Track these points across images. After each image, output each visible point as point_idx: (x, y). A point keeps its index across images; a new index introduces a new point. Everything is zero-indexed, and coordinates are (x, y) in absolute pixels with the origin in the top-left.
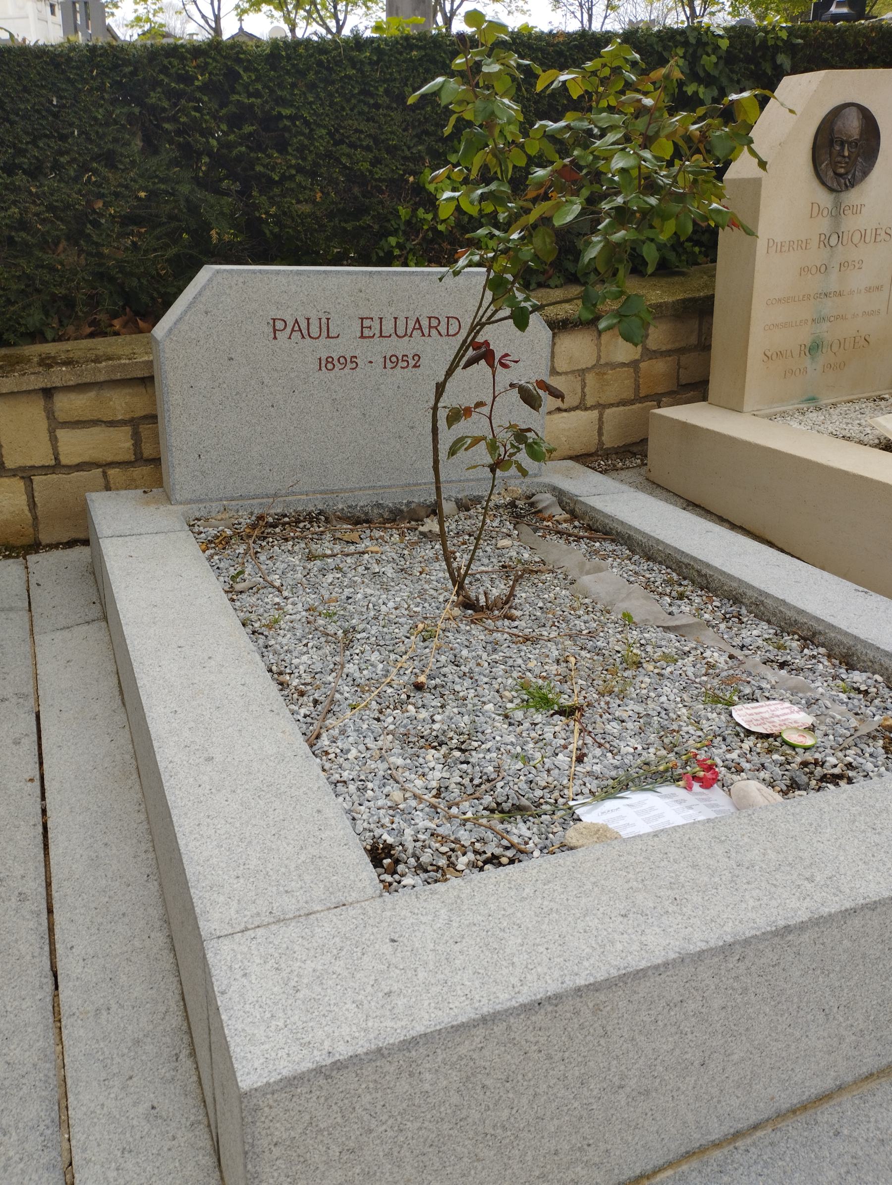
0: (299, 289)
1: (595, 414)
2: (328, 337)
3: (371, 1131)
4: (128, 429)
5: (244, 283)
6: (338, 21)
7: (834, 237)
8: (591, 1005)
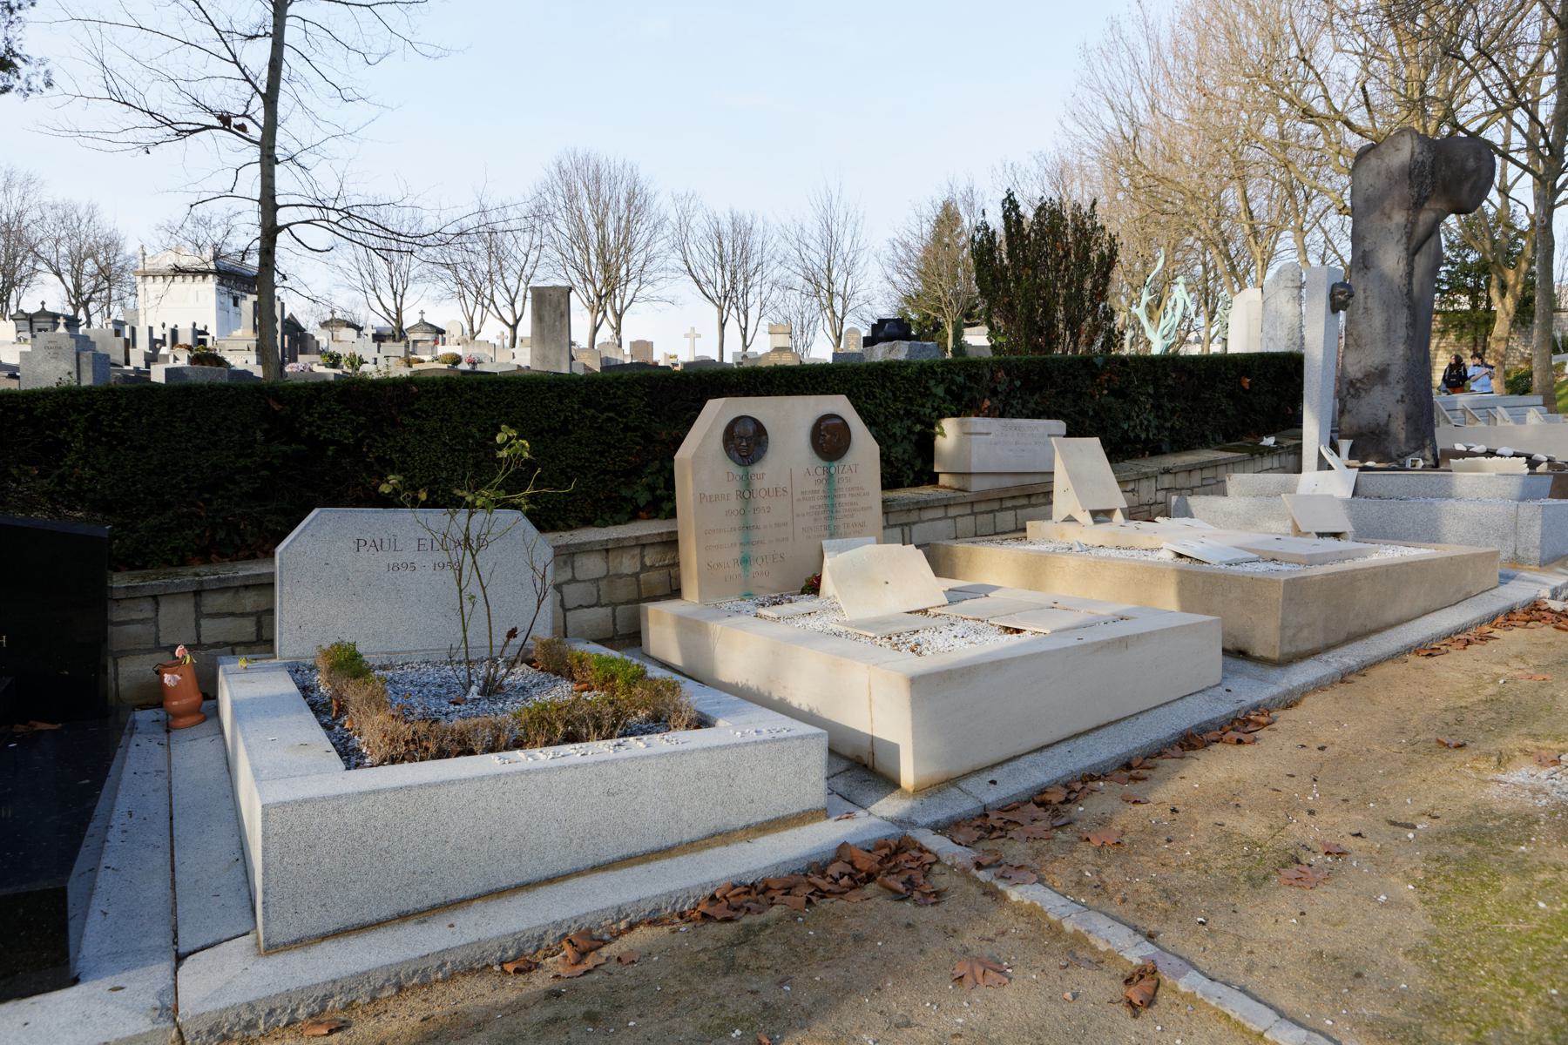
1: (609, 609)
4: (254, 619)
6: (514, 311)
7: (747, 492)
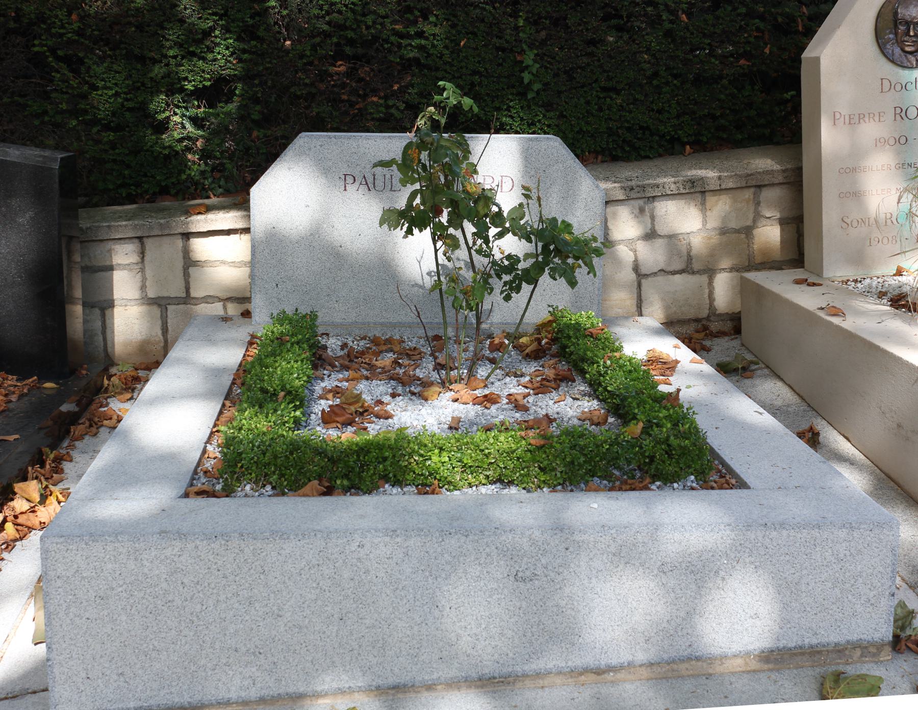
0: (367, 151)
2: (391, 190)
3: (113, 589)
5: (321, 146)
8: (252, 548)
